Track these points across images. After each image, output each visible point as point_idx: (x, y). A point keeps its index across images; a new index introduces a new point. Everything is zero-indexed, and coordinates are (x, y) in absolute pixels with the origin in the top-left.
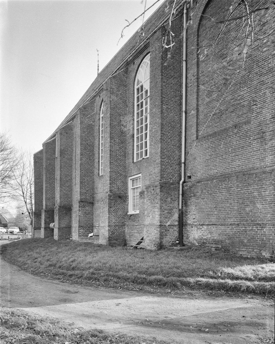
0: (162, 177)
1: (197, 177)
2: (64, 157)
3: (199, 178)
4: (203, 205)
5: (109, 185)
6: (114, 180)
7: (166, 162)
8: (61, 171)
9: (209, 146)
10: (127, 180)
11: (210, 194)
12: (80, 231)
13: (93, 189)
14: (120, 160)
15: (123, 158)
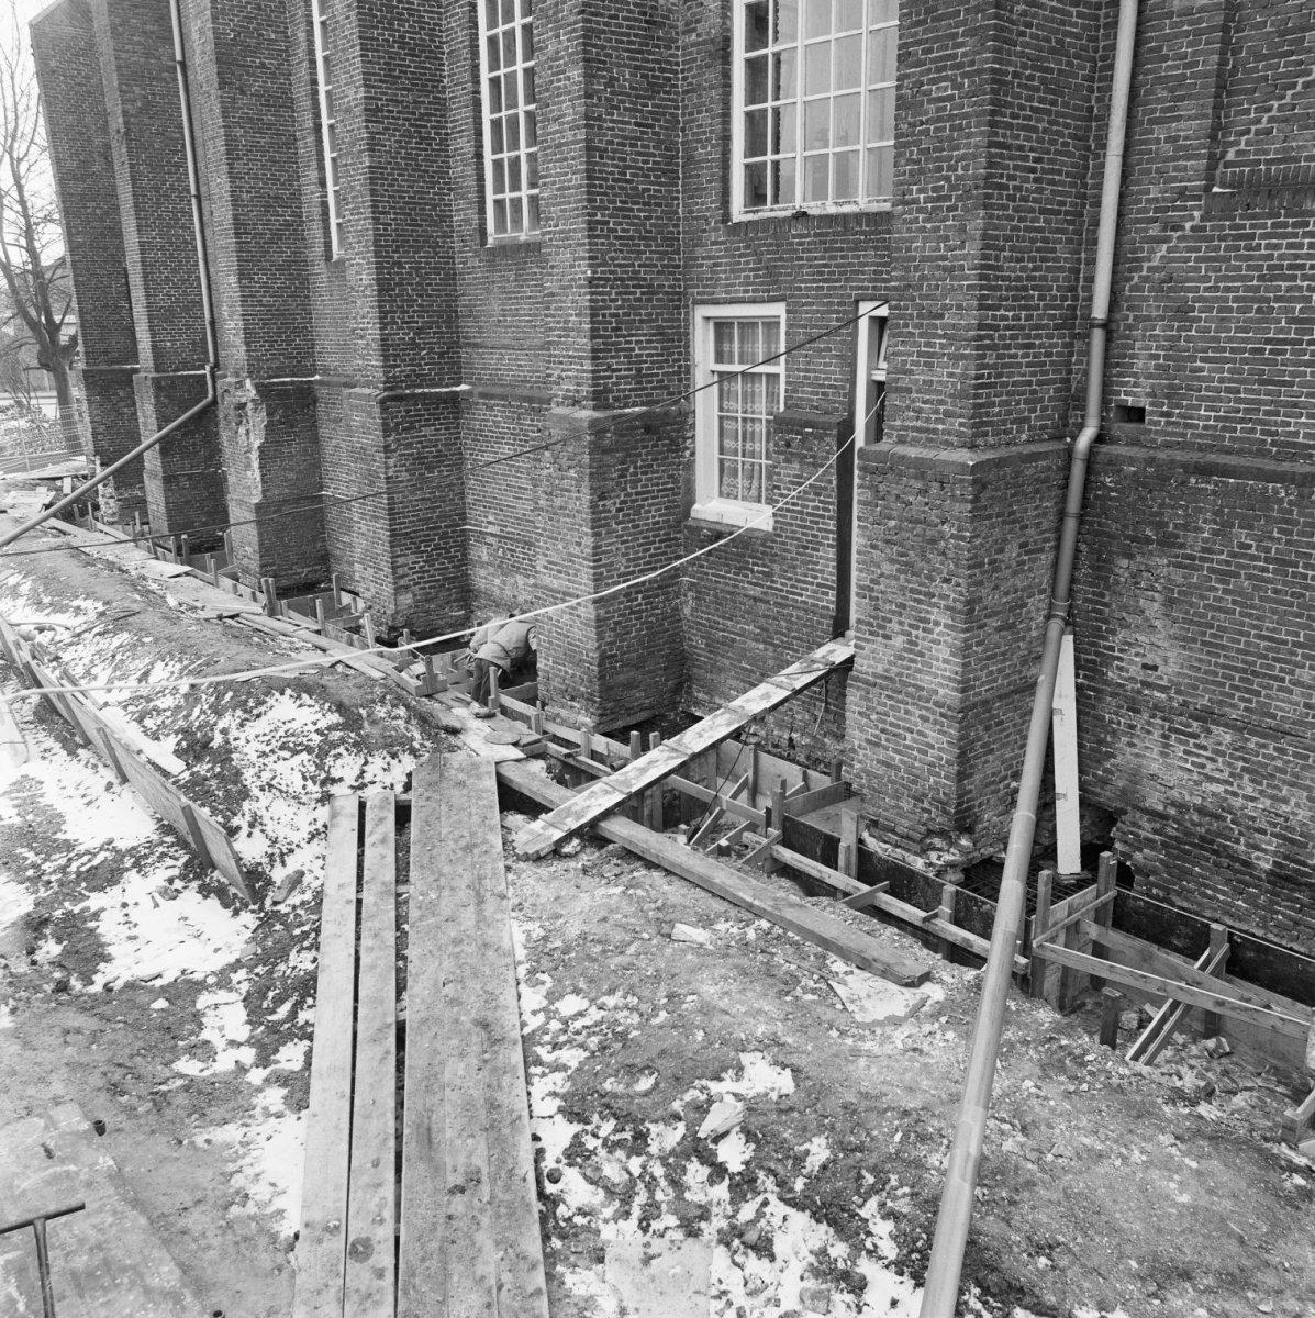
0: (983, 424)
1: (1188, 426)
2: (243, 92)
3: (1200, 436)
4: (1220, 609)
5: (588, 365)
6: (613, 329)
7: (1007, 328)
8: (233, 177)
9: (1297, 257)
10: (686, 320)
11: (1282, 563)
12: (401, 561)
13: (450, 316)
14: (645, 204)
15: (660, 184)
